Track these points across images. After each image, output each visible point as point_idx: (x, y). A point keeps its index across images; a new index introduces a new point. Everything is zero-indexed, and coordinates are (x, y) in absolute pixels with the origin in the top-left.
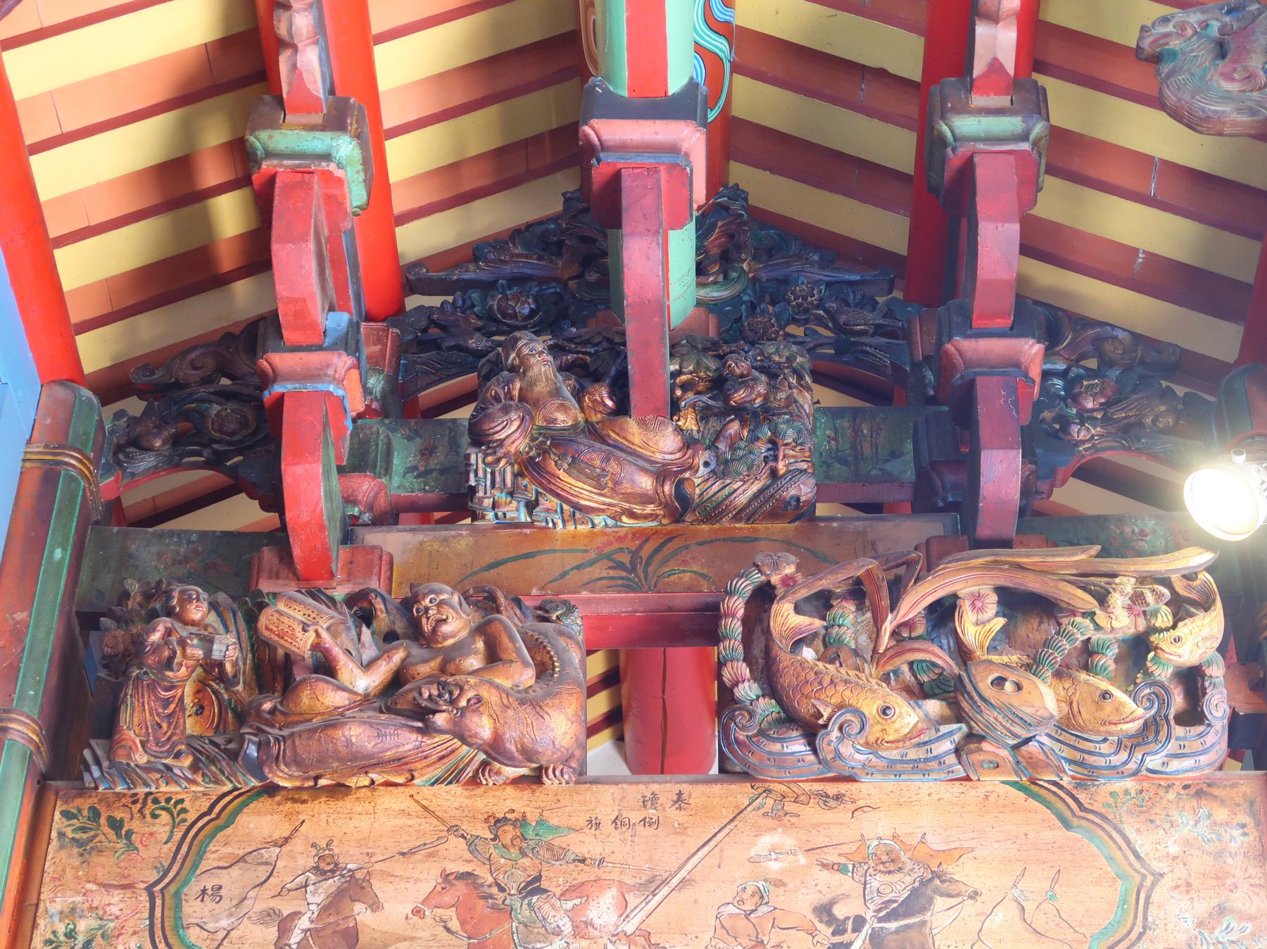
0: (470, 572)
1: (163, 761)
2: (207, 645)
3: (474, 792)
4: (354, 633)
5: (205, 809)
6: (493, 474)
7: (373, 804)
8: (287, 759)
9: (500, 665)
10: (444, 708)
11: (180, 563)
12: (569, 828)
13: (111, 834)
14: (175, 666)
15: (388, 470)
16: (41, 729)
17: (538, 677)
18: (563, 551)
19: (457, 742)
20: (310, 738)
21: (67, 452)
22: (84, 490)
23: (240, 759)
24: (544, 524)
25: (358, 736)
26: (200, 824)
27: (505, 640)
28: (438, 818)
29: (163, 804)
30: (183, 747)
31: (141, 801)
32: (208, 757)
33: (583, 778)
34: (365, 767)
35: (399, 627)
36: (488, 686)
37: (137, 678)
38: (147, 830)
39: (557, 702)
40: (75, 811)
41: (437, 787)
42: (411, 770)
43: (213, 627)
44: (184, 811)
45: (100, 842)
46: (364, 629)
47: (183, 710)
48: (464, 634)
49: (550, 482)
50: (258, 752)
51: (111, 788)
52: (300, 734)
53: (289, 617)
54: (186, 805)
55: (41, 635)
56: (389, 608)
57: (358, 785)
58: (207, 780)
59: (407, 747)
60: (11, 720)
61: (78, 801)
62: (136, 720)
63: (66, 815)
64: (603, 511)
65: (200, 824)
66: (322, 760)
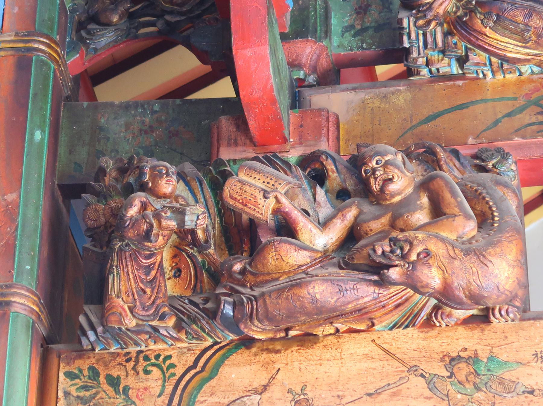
0: (409, 126)
1: (150, 323)
2: (179, 217)
3: (430, 334)
4: (309, 193)
5: (190, 363)
6: (425, 35)
7: (339, 350)
8: (260, 316)
9: (444, 221)
10: (397, 262)
11: (146, 132)
12: (517, 362)
13: (110, 390)
14: (153, 238)
15: (327, 33)
16: (39, 299)
17: (480, 226)
18: (493, 100)
19: (411, 292)
20: (278, 297)
21: (36, 38)
22: (55, 72)
23: (218, 319)
24: (475, 75)
25: (321, 293)
26: (187, 377)
27: (447, 195)
28: (398, 359)
29: (153, 361)
30: (166, 309)
31: (133, 359)
32: (189, 317)
33: (527, 315)
34: (329, 318)
35: (350, 185)
36: (435, 239)
37: (121, 250)
38: (142, 385)
39: (498, 250)
40: (77, 372)
41: (395, 331)
42: (371, 319)
43: (183, 198)
44: (172, 366)
45: (102, 398)
46: (318, 188)
47: (163, 274)
48: (410, 190)
49: (478, 39)
50: (234, 312)
51: (106, 349)
52: (270, 293)
53: (250, 185)
54: (174, 360)
55: (31, 212)
56: (340, 167)
57: (325, 333)
58: (190, 337)
59: (366, 299)
60: (14, 294)
61: (79, 363)
62: (123, 289)
63: (70, 375)
64: (529, 61)
65: (187, 377)
66: (291, 315)
